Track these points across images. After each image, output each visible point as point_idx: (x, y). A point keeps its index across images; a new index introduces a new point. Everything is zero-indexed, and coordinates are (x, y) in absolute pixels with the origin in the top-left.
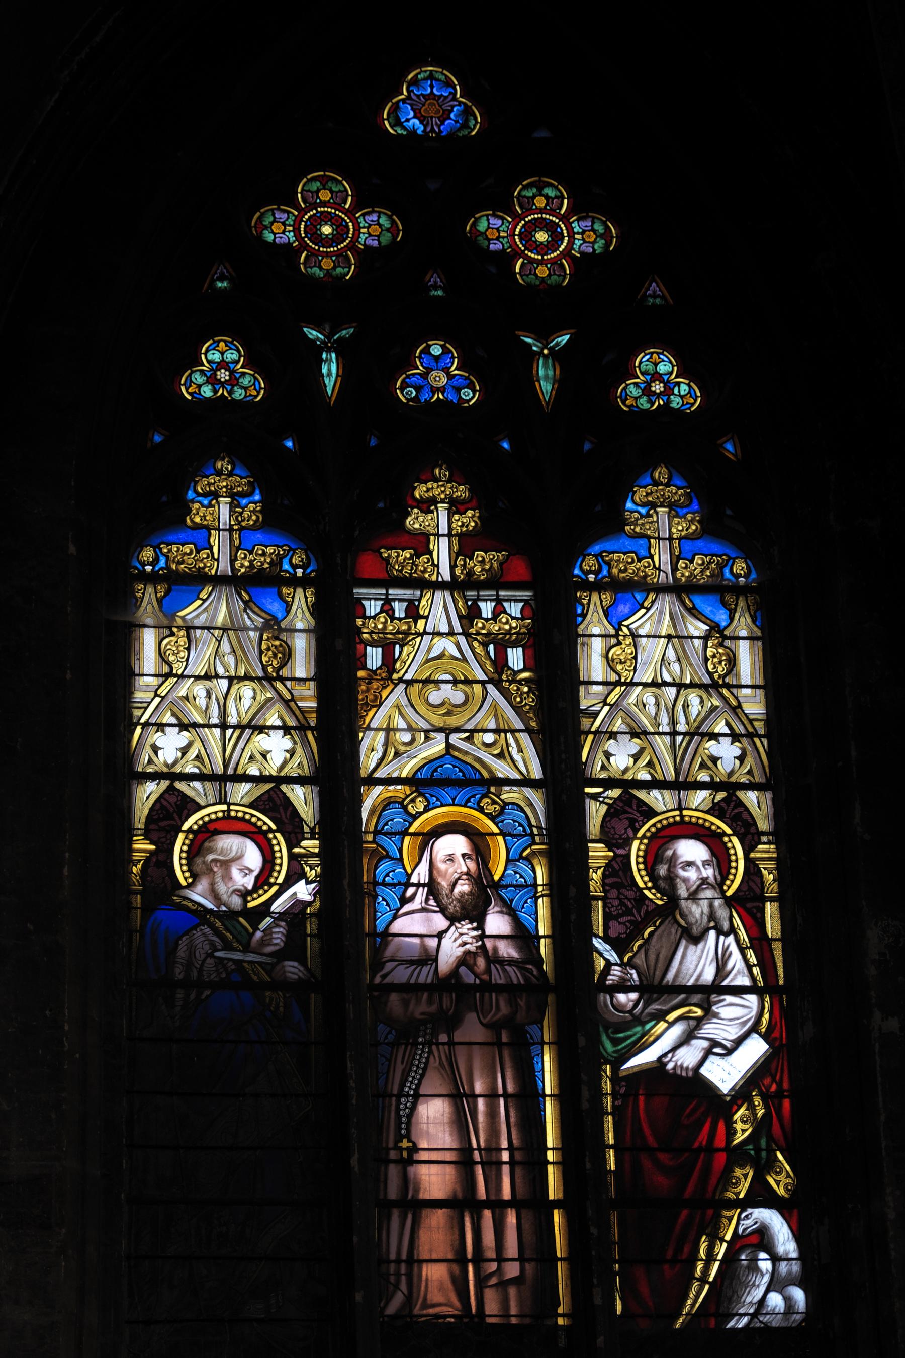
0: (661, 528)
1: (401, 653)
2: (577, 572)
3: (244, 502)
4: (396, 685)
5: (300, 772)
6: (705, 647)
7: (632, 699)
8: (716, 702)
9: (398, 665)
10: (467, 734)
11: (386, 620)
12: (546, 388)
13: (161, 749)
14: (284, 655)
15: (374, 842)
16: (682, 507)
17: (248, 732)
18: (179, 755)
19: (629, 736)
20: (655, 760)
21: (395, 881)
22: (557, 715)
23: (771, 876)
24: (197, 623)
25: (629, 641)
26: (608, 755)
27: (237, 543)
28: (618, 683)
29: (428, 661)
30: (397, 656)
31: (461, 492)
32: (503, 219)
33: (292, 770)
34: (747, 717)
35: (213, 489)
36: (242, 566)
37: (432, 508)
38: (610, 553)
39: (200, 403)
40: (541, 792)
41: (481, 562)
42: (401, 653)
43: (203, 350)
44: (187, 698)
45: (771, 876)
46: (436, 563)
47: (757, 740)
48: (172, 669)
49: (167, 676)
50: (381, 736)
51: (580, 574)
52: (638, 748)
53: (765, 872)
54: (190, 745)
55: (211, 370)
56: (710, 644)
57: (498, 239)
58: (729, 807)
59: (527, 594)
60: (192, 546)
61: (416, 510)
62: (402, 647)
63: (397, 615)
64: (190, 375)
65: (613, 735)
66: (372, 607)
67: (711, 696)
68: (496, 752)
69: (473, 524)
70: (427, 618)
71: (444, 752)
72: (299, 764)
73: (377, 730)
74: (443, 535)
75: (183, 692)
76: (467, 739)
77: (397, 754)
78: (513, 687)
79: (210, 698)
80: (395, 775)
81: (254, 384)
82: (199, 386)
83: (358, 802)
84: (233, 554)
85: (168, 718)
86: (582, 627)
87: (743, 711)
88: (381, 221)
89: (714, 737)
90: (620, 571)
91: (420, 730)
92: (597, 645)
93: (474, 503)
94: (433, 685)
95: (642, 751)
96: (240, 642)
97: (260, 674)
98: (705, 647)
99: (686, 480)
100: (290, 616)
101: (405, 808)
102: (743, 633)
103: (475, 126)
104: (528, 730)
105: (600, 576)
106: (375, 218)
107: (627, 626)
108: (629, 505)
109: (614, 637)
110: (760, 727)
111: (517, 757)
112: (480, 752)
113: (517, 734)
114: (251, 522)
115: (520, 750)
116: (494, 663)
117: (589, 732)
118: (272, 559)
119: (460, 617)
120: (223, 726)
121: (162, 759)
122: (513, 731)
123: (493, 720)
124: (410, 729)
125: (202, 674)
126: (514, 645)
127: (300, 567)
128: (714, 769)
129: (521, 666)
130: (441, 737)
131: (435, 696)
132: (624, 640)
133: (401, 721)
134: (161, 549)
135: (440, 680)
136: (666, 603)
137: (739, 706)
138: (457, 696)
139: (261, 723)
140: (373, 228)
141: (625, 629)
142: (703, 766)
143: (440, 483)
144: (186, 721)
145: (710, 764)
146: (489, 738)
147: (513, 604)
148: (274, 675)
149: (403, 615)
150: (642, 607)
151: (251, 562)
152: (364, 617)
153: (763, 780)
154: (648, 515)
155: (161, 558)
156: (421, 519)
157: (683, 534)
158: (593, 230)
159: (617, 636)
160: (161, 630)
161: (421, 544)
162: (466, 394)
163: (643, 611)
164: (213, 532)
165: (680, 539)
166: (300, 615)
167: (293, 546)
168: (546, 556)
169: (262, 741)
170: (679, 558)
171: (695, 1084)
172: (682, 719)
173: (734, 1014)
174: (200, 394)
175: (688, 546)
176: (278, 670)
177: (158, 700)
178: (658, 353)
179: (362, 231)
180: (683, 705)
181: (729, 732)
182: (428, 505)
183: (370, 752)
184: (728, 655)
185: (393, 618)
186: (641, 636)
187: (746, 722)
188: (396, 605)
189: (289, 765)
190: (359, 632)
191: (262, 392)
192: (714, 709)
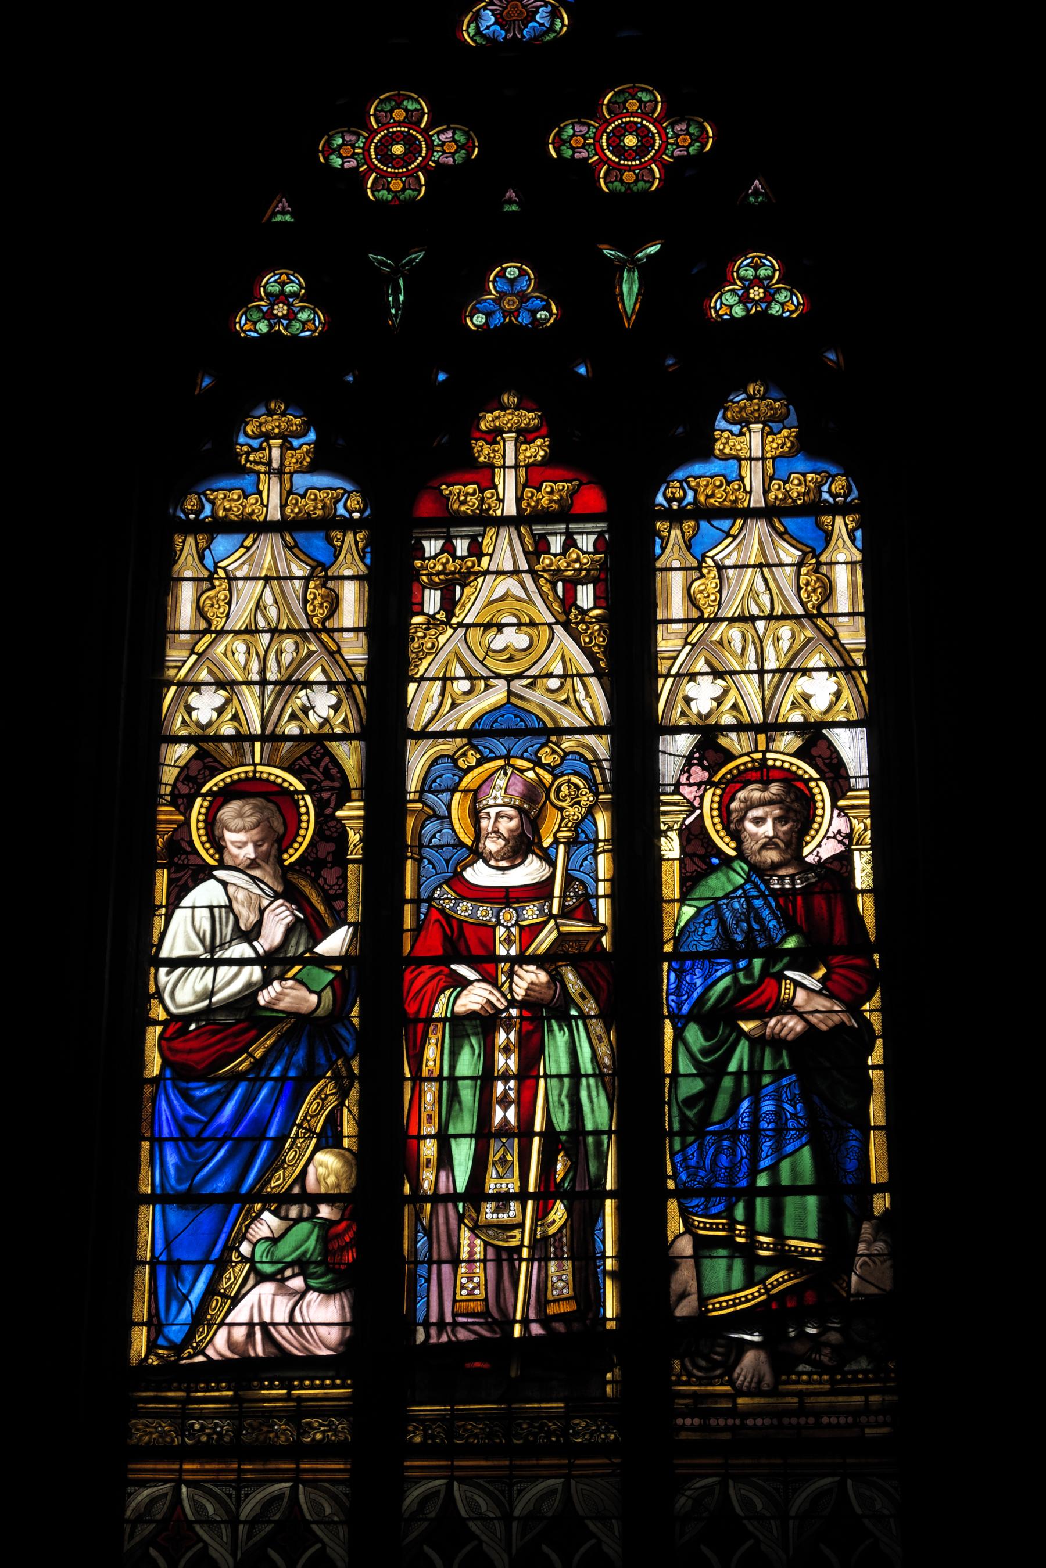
0: (751, 451)
1: (462, 595)
2: (660, 499)
3: (296, 443)
4: (455, 629)
6: (306, 588)
7: (220, 648)
8: (809, 633)
10: (530, 680)
11: (448, 560)
15: (420, 801)
17: (288, 689)
18: (715, 704)
19: (711, 678)
21: (442, 843)
23: (358, 836)
25: (714, 573)
26: (688, 700)
27: (770, 471)
28: (701, 619)
31: (528, 418)
32: (589, 125)
34: (845, 649)
40: (606, 739)
42: (462, 595)
44: (720, 642)
45: (358, 837)
47: (355, 687)
48: (703, 613)
50: (438, 684)
53: (351, 833)
54: (726, 692)
55: (742, 288)
56: (312, 584)
57: (583, 147)
59: (602, 526)
60: (475, 486)
62: (462, 589)
63: (459, 554)
64: (720, 297)
65: (692, 677)
66: (432, 547)
69: (308, 460)
70: (491, 555)
71: (505, 701)
74: (509, 467)
75: (716, 637)
77: (454, 705)
79: (249, 654)
80: (451, 728)
81: (791, 299)
82: (731, 307)
84: (284, 498)
85: (204, 676)
86: (662, 559)
88: (457, 138)
90: (708, 497)
91: (482, 677)
92: (677, 580)
93: (544, 431)
95: (726, 692)
98: (306, 588)
100: (830, 548)
101: (455, 761)
102: (348, 572)
104: (598, 674)
106: (450, 135)
107: (712, 558)
108: (242, 439)
110: (859, 659)
111: (586, 704)
114: (786, 449)
115: (588, 695)
116: (563, 602)
117: (667, 676)
118: (561, 496)
119: (526, 553)
121: (695, 710)
122: (581, 676)
123: (458, 665)
124: (469, 677)
125: (736, 615)
126: (584, 582)
129: (591, 605)
130: (502, 684)
131: (499, 643)
132: (708, 573)
135: (504, 633)
136: (759, 528)
139: (194, 680)
140: (447, 145)
141: (710, 562)
142: (293, 717)
143: (275, 417)
144: (721, 669)
145: (301, 715)
148: (320, 626)
149: (465, 553)
152: (424, 559)
153: (358, 729)
154: (261, 448)
156: (731, 443)
157: (531, 460)
158: (454, 140)
159: (699, 568)
161: (485, 476)
162: (479, 319)
163: (730, 539)
165: (774, 458)
170: (772, 478)
172: (275, 668)
177: (194, 657)
178: (760, 258)
179: (591, 141)
180: (276, 652)
181: (709, 670)
182: (494, 435)
183: (423, 704)
184: (822, 582)
185: (455, 557)
186: (237, 579)
189: (836, 709)
190: (417, 573)
192: (310, 654)
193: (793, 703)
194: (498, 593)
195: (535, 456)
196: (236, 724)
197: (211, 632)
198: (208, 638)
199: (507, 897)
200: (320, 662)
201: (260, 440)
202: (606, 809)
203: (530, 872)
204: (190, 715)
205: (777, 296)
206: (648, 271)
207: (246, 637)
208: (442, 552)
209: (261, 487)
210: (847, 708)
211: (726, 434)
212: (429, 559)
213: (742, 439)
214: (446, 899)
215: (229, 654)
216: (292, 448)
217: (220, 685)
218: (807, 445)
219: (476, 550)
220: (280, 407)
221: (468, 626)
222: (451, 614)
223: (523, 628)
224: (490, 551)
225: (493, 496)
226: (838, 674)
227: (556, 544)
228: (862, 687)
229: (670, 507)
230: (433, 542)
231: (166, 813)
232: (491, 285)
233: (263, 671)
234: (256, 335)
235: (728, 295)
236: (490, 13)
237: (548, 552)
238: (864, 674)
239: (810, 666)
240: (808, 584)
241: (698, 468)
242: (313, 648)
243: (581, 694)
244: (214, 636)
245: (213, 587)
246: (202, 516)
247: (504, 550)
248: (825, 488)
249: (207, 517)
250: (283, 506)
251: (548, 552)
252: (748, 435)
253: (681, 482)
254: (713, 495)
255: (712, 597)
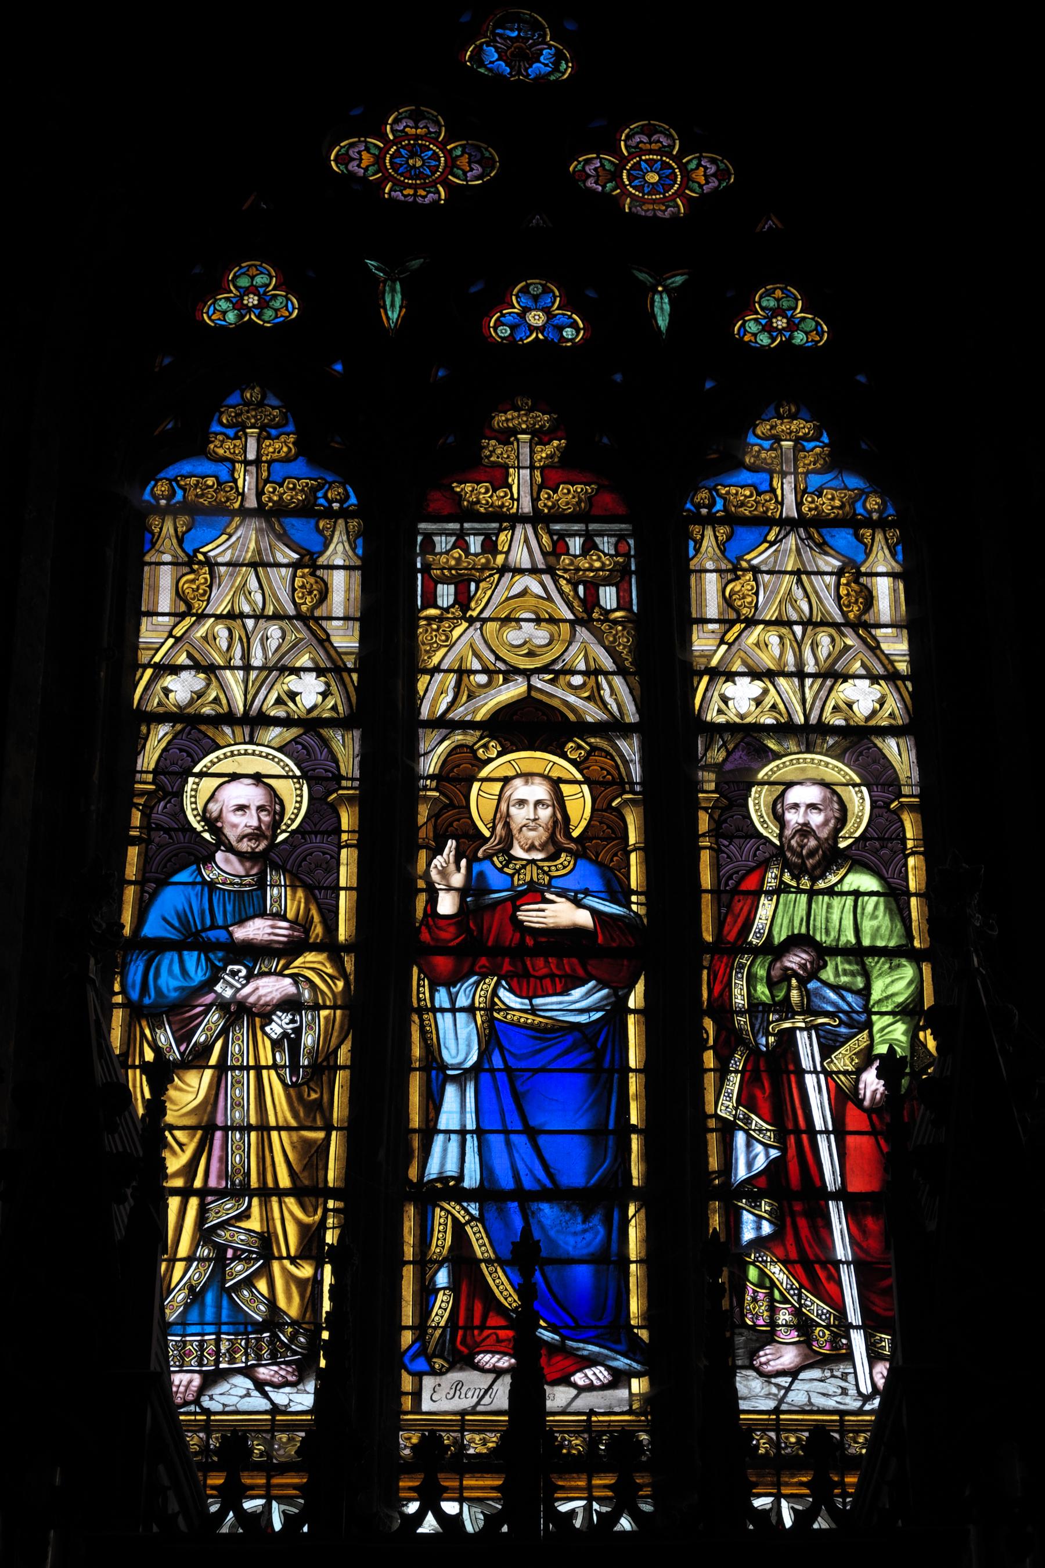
0: (786, 466)
5: (893, 722)
7: (201, 632)
9: (473, 605)
13: (730, 699)
14: (320, 593)
16: (809, 440)
20: (222, 696)
22: (660, 656)
24: (220, 560)
25: (749, 576)
26: (725, 700)
27: (265, 474)
28: (738, 620)
29: (508, 599)
30: (472, 593)
33: (882, 720)
35: (511, 425)
36: (270, 500)
37: (512, 439)
38: (186, 477)
39: (222, 330)
41: (567, 496)
43: (757, 299)
46: (516, 496)
47: (345, 675)
49: (182, 616)
50: (452, 678)
51: (693, 508)
52: (761, 691)
54: (766, 692)
56: (299, 573)
61: (493, 442)
63: (472, 551)
66: (442, 543)
67: (846, 636)
68: (586, 694)
73: (449, 671)
76: (551, 682)
77: (470, 697)
78: (605, 627)
79: (231, 638)
85: (182, 659)
87: (332, 644)
89: (296, 671)
94: (514, 624)
96: (813, 587)
97: (291, 611)
99: (281, 400)
100: (871, 559)
102: (881, 569)
103: (566, 70)
105: (174, 501)
109: (734, 571)
110: (903, 667)
112: (568, 697)
113: (610, 677)
116: (583, 602)
119: (544, 554)
120: (247, 668)
122: (606, 673)
124: (485, 670)
125: (225, 612)
127: (337, 501)
128: (291, 704)
129: (614, 606)
133: (475, 660)
134: (717, 491)
135: (515, 618)
137: (878, 647)
138: (541, 635)
141: (201, 557)
146: (577, 680)
147: (606, 539)
150: (765, 541)
151: (281, 496)
155: (718, 499)
156: (499, 451)
160: (180, 568)
161: (499, 479)
163: (766, 545)
164: (511, 470)
165: (270, 463)
167: (329, 479)
169: (847, 690)
174: (756, 342)
175: (279, 470)
176: (858, 617)
182: (507, 436)
185: (467, 552)
187: (886, 662)
188: (471, 539)
191: (826, 335)
193: (834, 708)
194: (516, 589)
195: (279, 452)
196: (774, 714)
197: (192, 615)
198: (188, 621)
200: (185, 648)
201: (771, 442)
202: (351, 805)
204: (167, 696)
205: (802, 325)
207: (228, 622)
208: (454, 547)
209: (236, 475)
210: (892, 715)
211: (756, 448)
212: (441, 554)
213: (237, 442)
215: (762, 645)
216: (804, 450)
217: (197, 667)
218: (838, 461)
219: (490, 547)
220: (527, 404)
221: (485, 621)
222: (465, 607)
223: (543, 624)
224: (505, 549)
225: (506, 495)
226: (764, 679)
227: (575, 545)
228: (351, 689)
229: (871, 518)
230: (443, 538)
232: (514, 298)
233: (246, 655)
234: (224, 323)
235: (752, 324)
236: (493, 49)
237: (567, 553)
238: (355, 676)
239: (298, 665)
240: (303, 587)
241: (186, 467)
242: (849, 642)
243: (606, 693)
244: (194, 619)
245: (738, 578)
246: (714, 510)
248: (320, 494)
249: (718, 511)
250: (799, 504)
251: (567, 553)
252: (515, 444)
253: (170, 481)
254: (202, 496)
255: (749, 599)
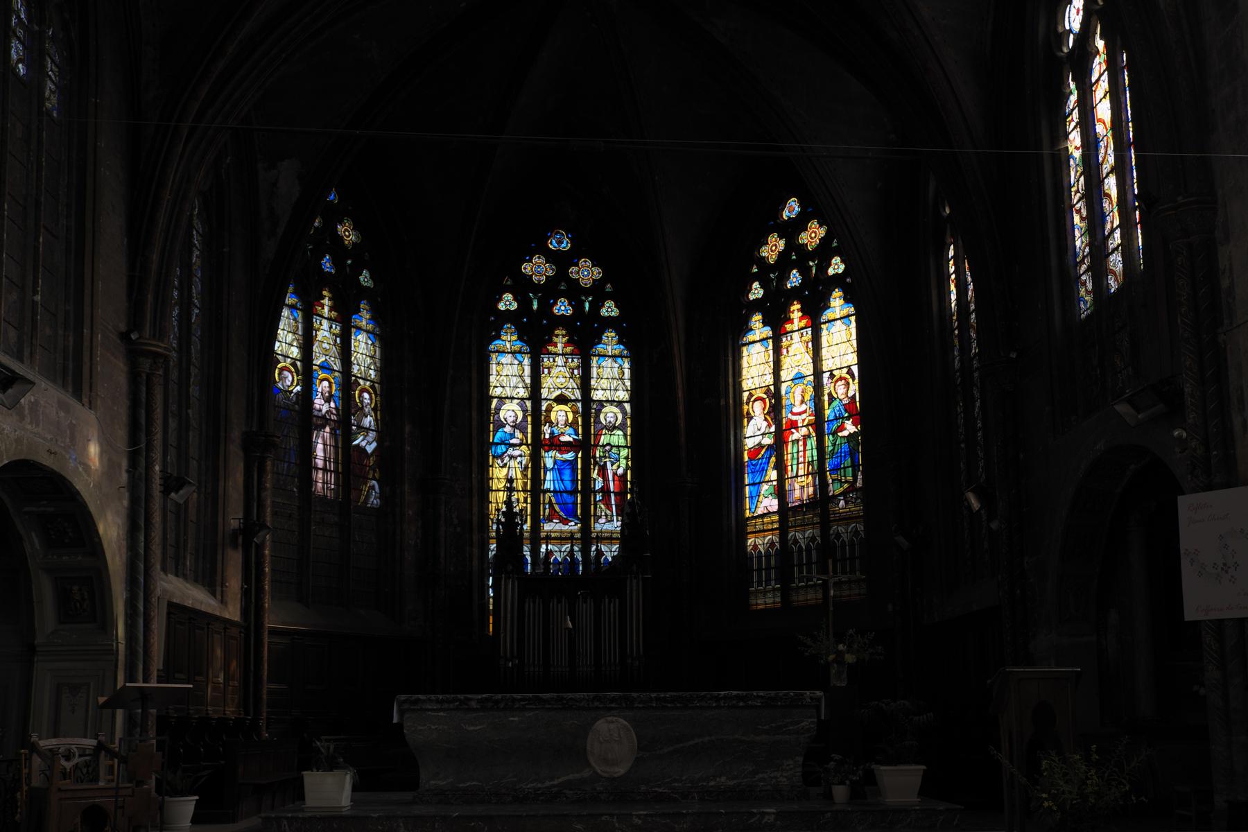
0: (610, 342)
12: (535, 307)
22: (585, 386)
41: (569, 349)
58: (372, 387)
72: (526, 395)
83: (541, 406)
112: (568, 394)
135: (559, 376)
161: (791, 321)
166: (527, 361)
168: (584, 349)
171: (364, 450)
173: (372, 435)
182: (557, 336)
183: (544, 393)
199: (800, 414)
203: (804, 407)
206: (590, 303)
214: (790, 416)
231: (745, 407)
247: (796, 336)
